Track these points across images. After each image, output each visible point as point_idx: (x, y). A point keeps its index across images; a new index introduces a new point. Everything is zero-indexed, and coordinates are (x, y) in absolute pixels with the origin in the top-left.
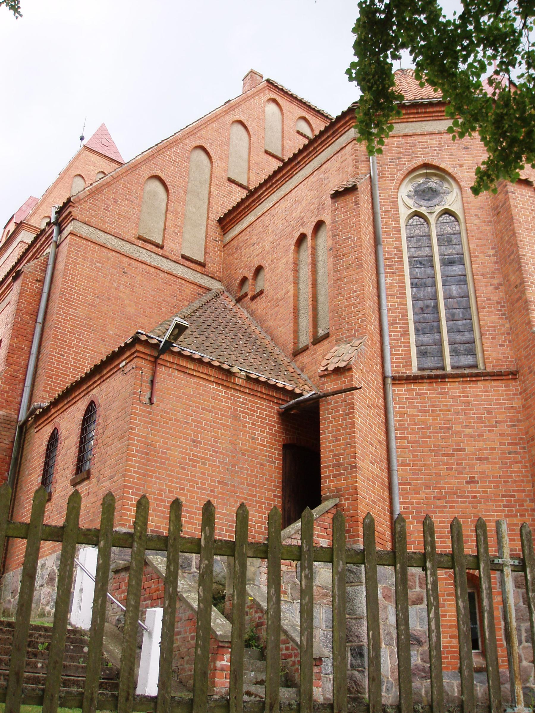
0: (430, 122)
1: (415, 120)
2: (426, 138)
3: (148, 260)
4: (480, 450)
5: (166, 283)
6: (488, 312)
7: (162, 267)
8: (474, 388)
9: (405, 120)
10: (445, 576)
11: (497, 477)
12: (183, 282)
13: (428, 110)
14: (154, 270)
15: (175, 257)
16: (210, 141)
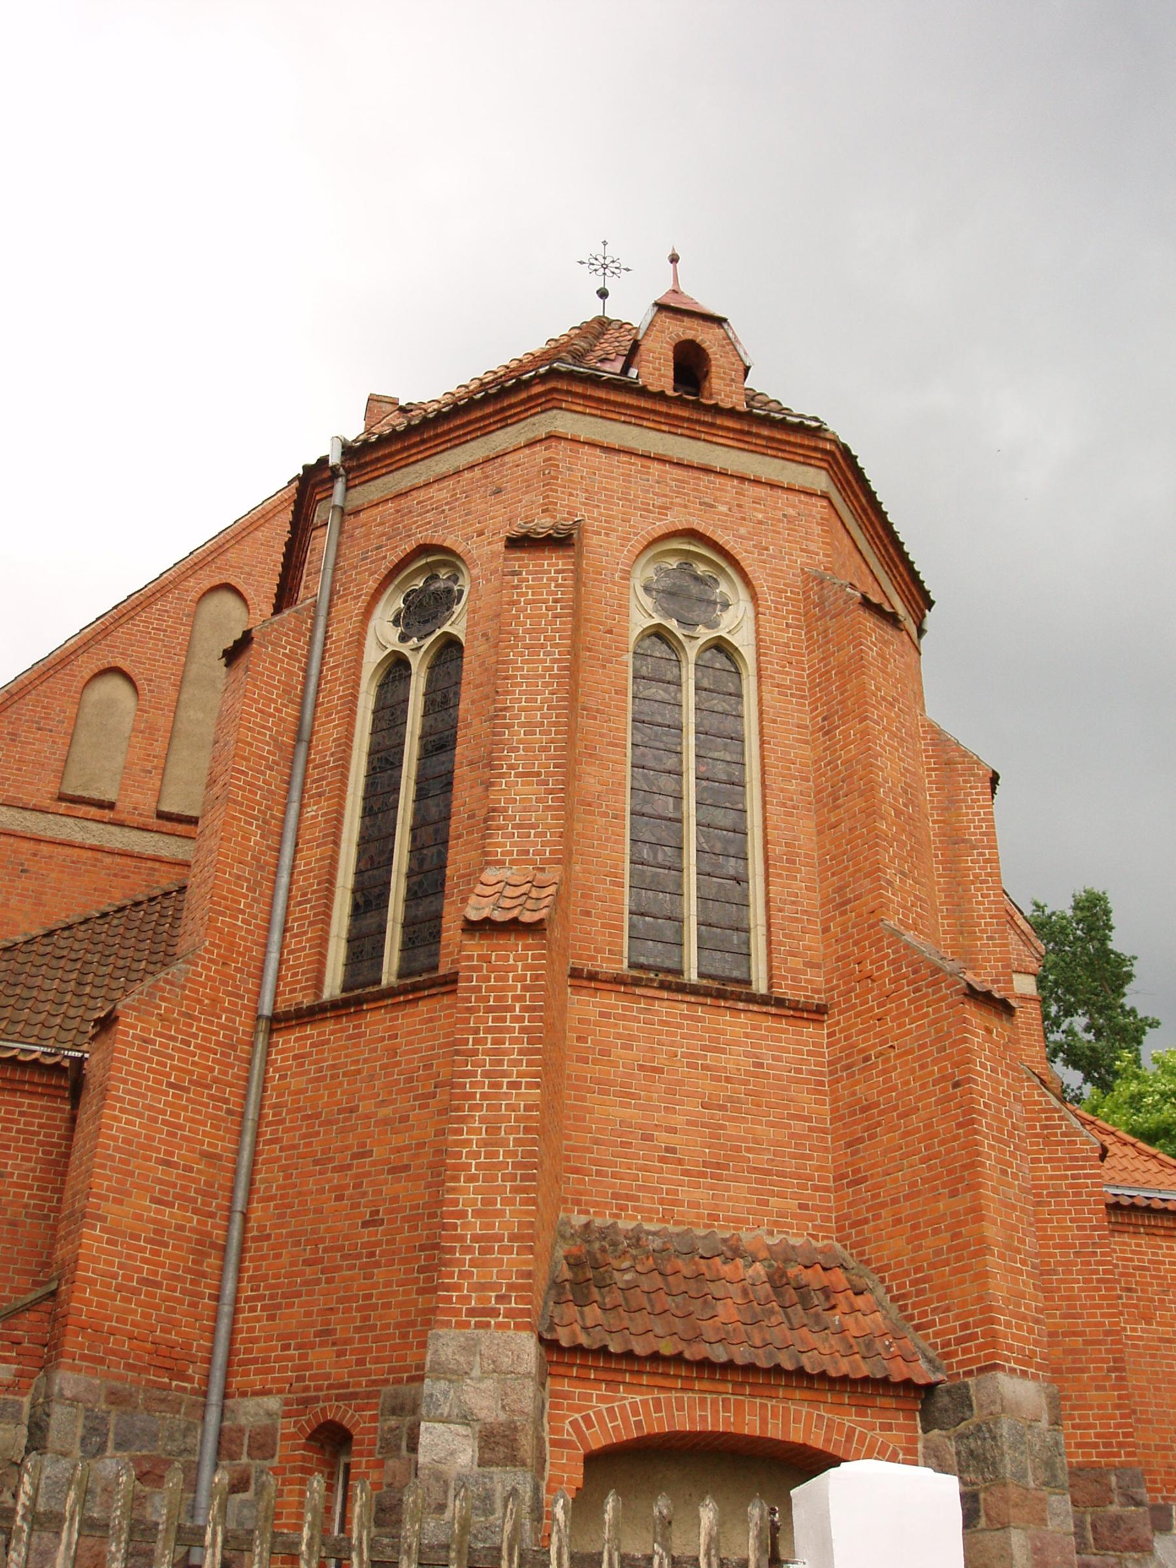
0: (446, 454)
1: (420, 456)
2: (432, 491)
3: (78, 837)
4: (398, 1150)
5: (115, 875)
6: (466, 843)
7: (108, 845)
8: (411, 1015)
9: (403, 463)
10: (292, 1430)
11: (417, 1207)
12: (157, 865)
13: (439, 430)
14: (90, 854)
15: (142, 819)
16: (247, 569)
